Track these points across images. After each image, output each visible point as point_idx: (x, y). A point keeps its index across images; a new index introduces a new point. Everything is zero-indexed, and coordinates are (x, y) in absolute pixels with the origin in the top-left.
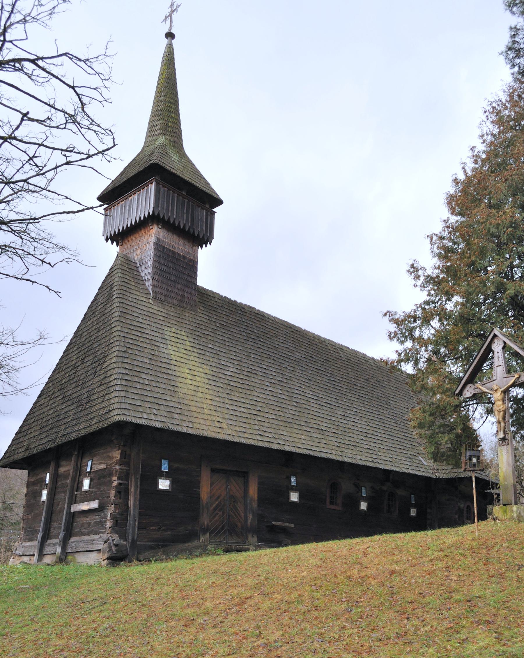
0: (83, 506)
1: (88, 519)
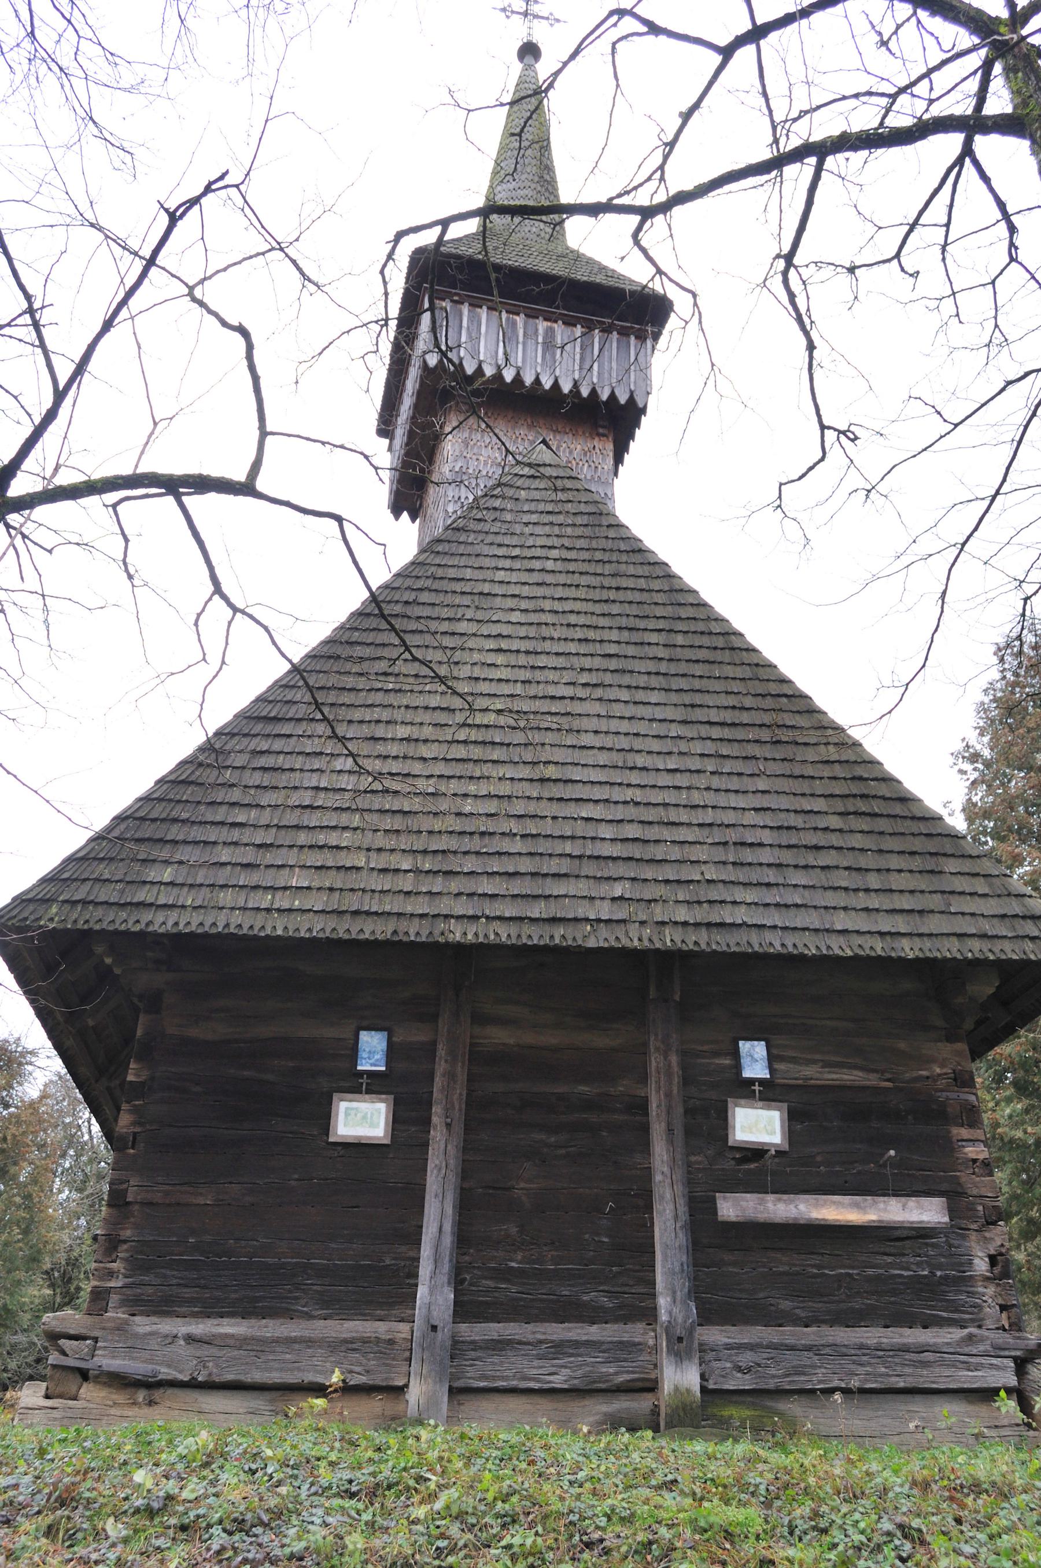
0: (816, 1206)
1: (816, 1260)
